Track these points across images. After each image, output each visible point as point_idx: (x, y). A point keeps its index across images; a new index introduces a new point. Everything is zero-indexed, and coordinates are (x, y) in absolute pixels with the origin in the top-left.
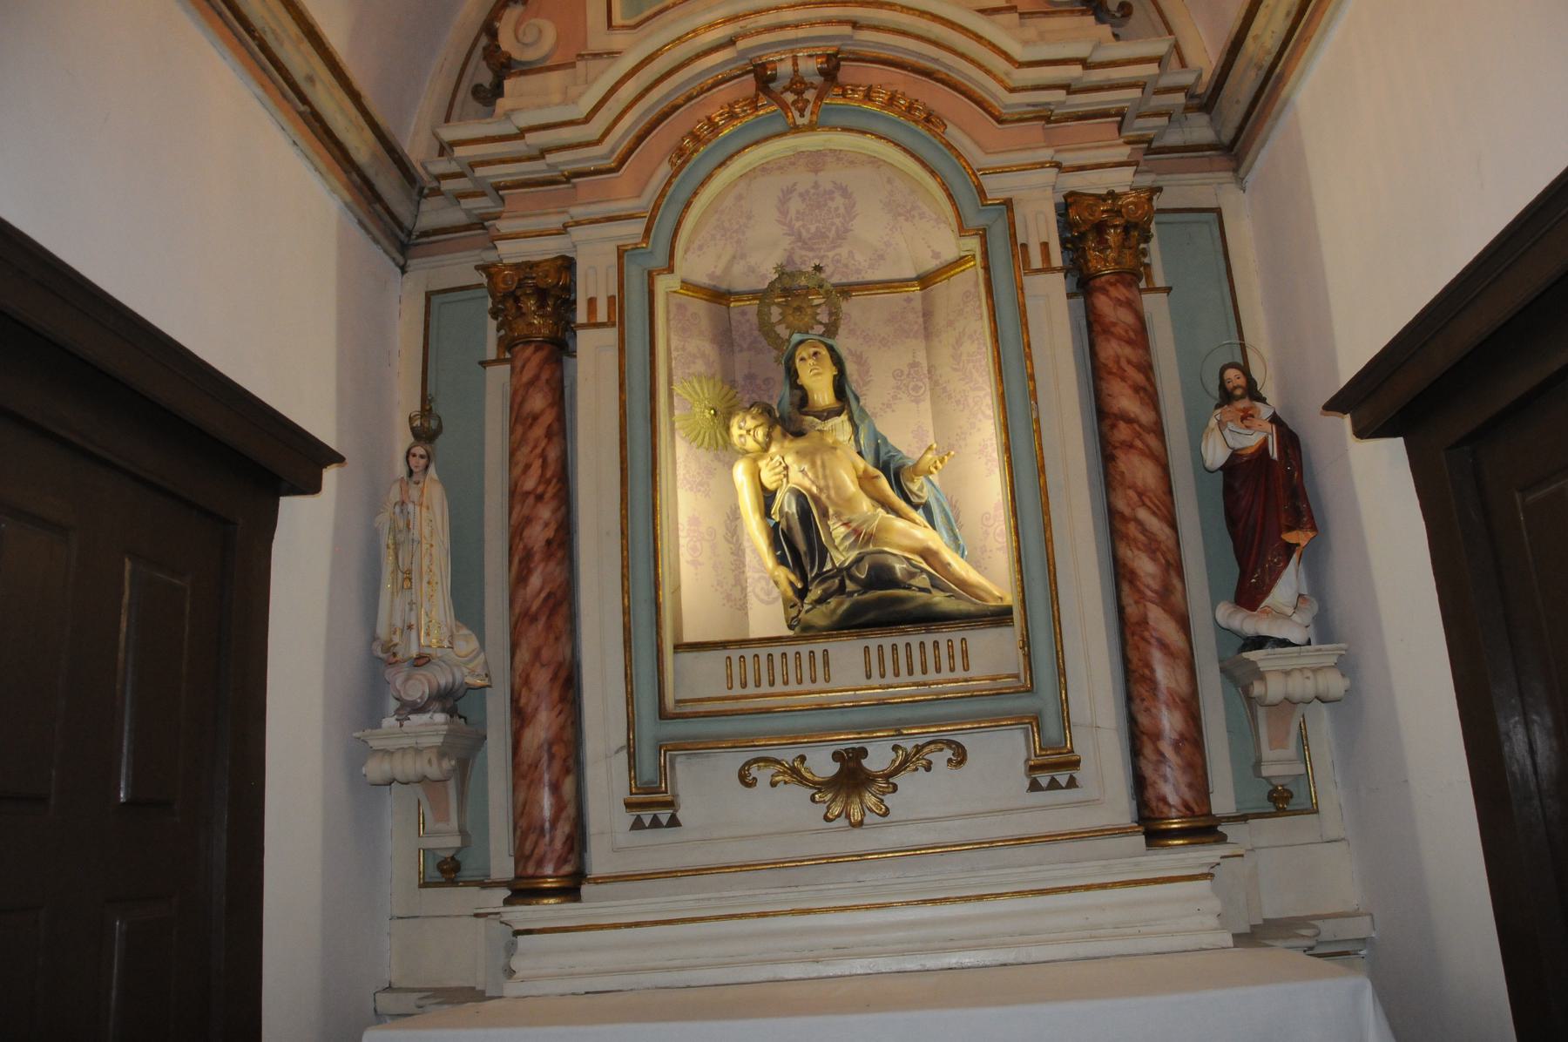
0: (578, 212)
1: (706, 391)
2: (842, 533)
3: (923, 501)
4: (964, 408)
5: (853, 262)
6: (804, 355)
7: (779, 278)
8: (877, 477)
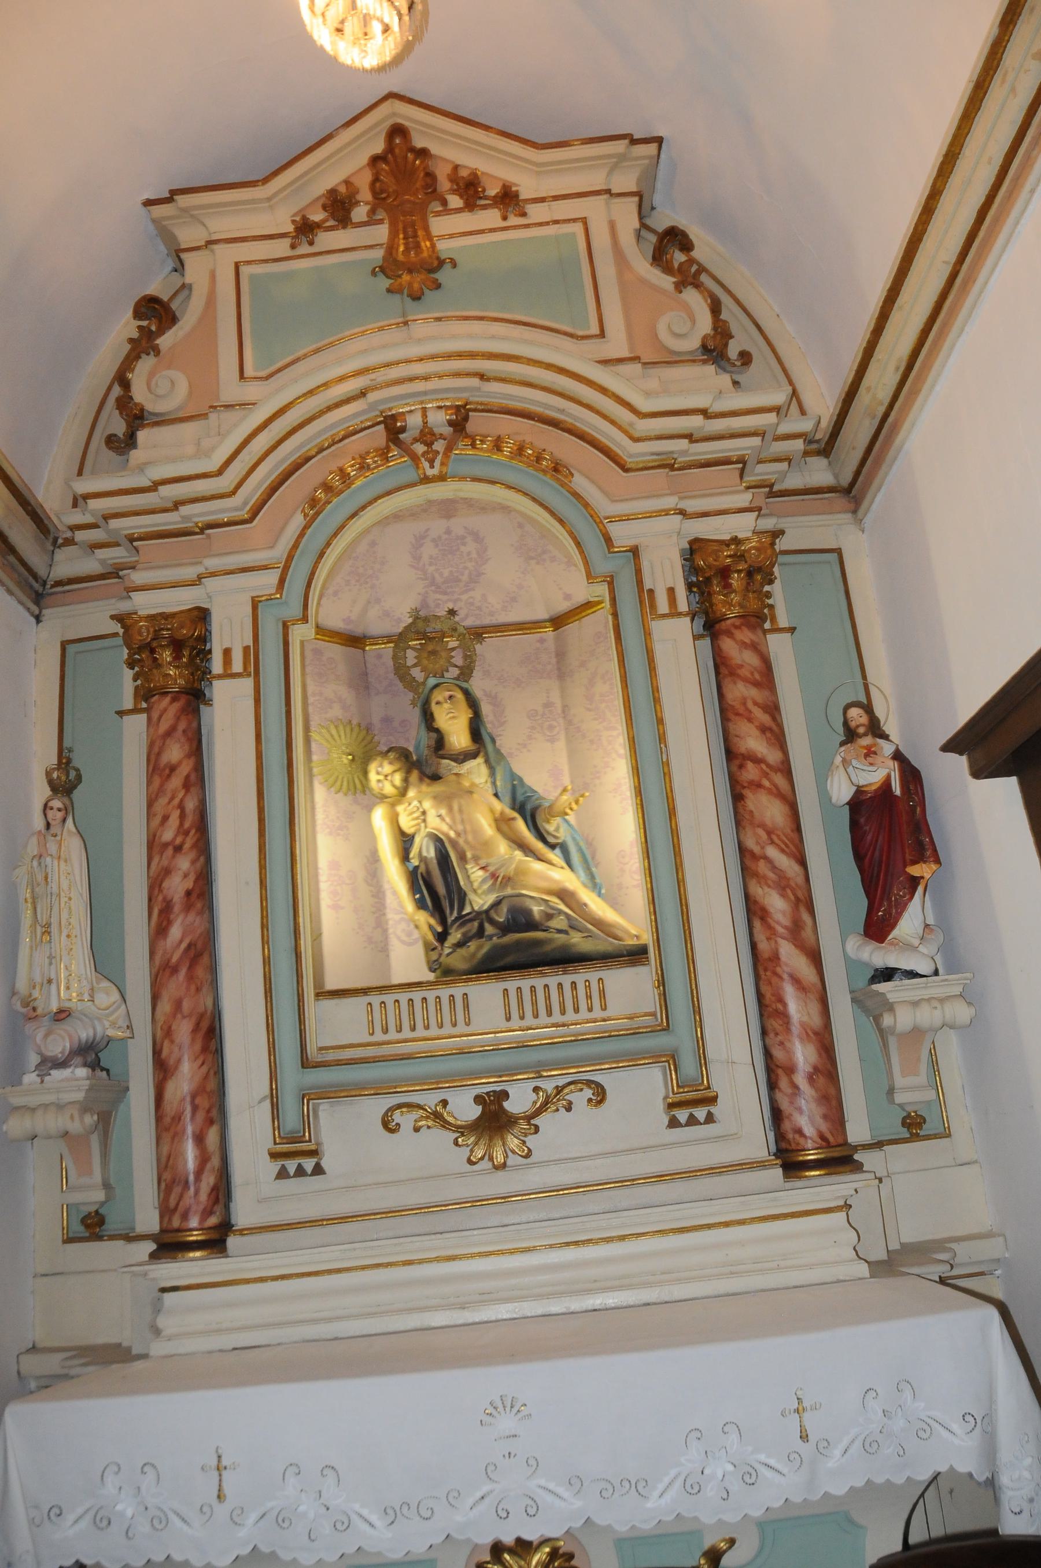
0: (213, 563)
2: (480, 877)
3: (560, 841)
6: (440, 698)
8: (513, 819)
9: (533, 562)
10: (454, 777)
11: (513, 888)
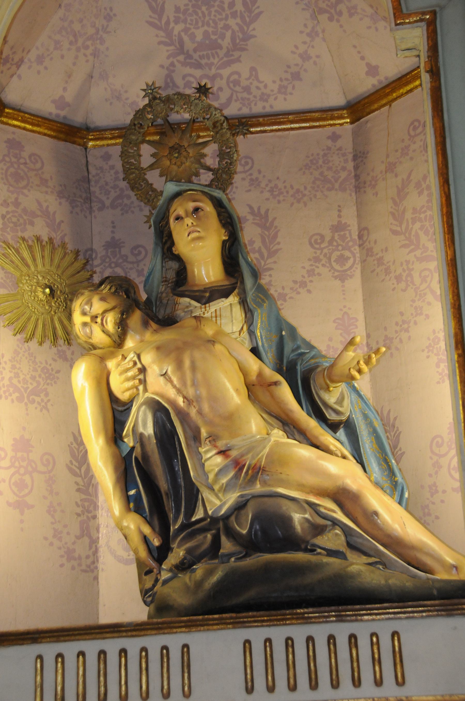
1: (39, 261)
2: (217, 465)
3: (344, 418)
4: (407, 286)
5: (255, 83)
6: (181, 212)
7: (149, 105)
8: (276, 383)
9: (323, 18)
10: (193, 322)
11: (264, 483)
